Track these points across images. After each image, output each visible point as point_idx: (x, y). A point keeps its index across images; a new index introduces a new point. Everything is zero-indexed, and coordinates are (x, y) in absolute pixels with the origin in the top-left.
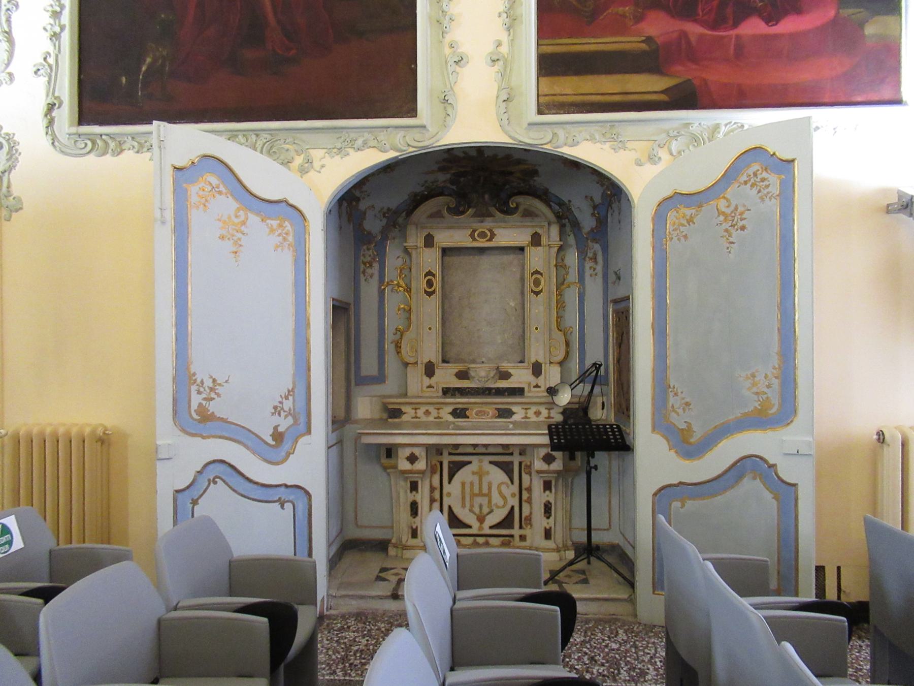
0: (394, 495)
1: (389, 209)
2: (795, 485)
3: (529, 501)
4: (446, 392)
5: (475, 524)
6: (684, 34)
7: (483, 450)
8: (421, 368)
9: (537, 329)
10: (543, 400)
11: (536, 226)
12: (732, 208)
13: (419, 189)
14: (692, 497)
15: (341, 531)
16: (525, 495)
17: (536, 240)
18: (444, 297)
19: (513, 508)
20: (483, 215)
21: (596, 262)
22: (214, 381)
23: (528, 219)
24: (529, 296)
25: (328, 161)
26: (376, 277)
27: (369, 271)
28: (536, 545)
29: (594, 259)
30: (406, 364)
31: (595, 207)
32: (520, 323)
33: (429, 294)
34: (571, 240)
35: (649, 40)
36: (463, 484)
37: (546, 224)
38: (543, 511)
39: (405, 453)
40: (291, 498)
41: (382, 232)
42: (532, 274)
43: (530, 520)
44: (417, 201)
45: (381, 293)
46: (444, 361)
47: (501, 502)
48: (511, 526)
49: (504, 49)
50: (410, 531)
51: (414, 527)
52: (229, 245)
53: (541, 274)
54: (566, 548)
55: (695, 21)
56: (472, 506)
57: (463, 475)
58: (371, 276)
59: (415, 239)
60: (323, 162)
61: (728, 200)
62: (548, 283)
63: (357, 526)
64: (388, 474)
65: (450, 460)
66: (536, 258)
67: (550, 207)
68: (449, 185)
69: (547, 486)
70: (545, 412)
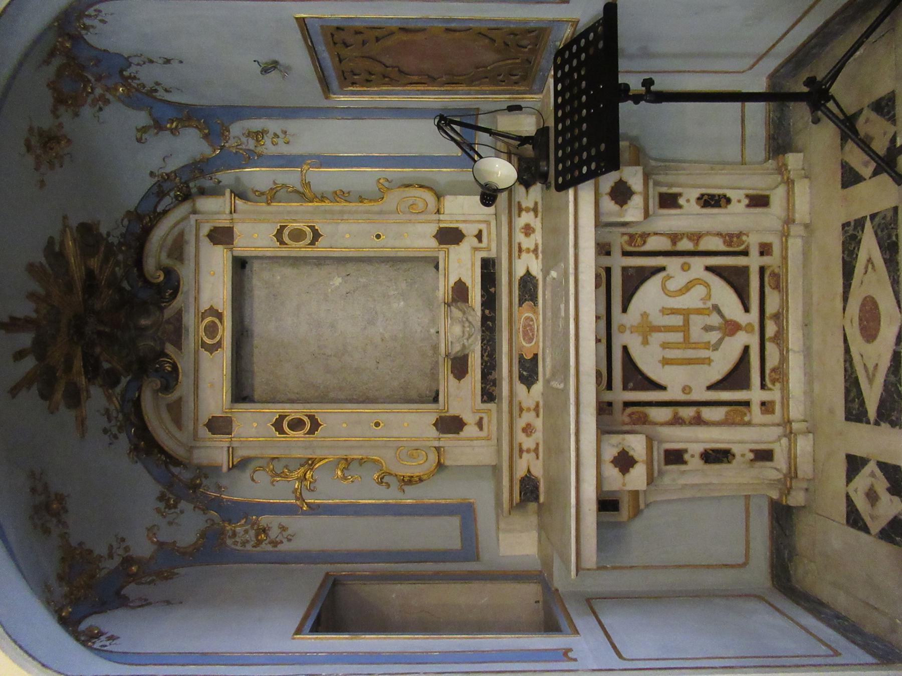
0: (688, 494)
1: (162, 498)
3: (696, 237)
4: (489, 394)
5: (741, 339)
8: (448, 441)
9: (378, 236)
10: (504, 219)
11: (198, 230)
13: (124, 442)
15: (760, 598)
16: (685, 245)
17: (222, 236)
18: (324, 399)
19: (708, 269)
20: (177, 333)
21: (263, 132)
24: (321, 249)
26: (284, 520)
27: (274, 533)
28: (778, 225)
29: (258, 135)
30: (440, 466)
31: (158, 126)
32: (369, 268)
34: (226, 177)
36: (666, 362)
37: (193, 218)
38: (715, 211)
39: (614, 478)
41: (205, 510)
42: (282, 243)
43: (731, 236)
44: (146, 445)
45: (315, 510)
46: (436, 400)
47: (700, 290)
48: (744, 271)
51: (751, 456)
53: (283, 228)
54: (782, 169)
56: (707, 346)
57: (648, 362)
58: (283, 528)
59: (215, 451)
62: (299, 214)
63: (744, 565)
64: (647, 506)
65: (626, 388)
67: (165, 212)
68: (119, 389)
69: (669, 201)
70: (527, 218)
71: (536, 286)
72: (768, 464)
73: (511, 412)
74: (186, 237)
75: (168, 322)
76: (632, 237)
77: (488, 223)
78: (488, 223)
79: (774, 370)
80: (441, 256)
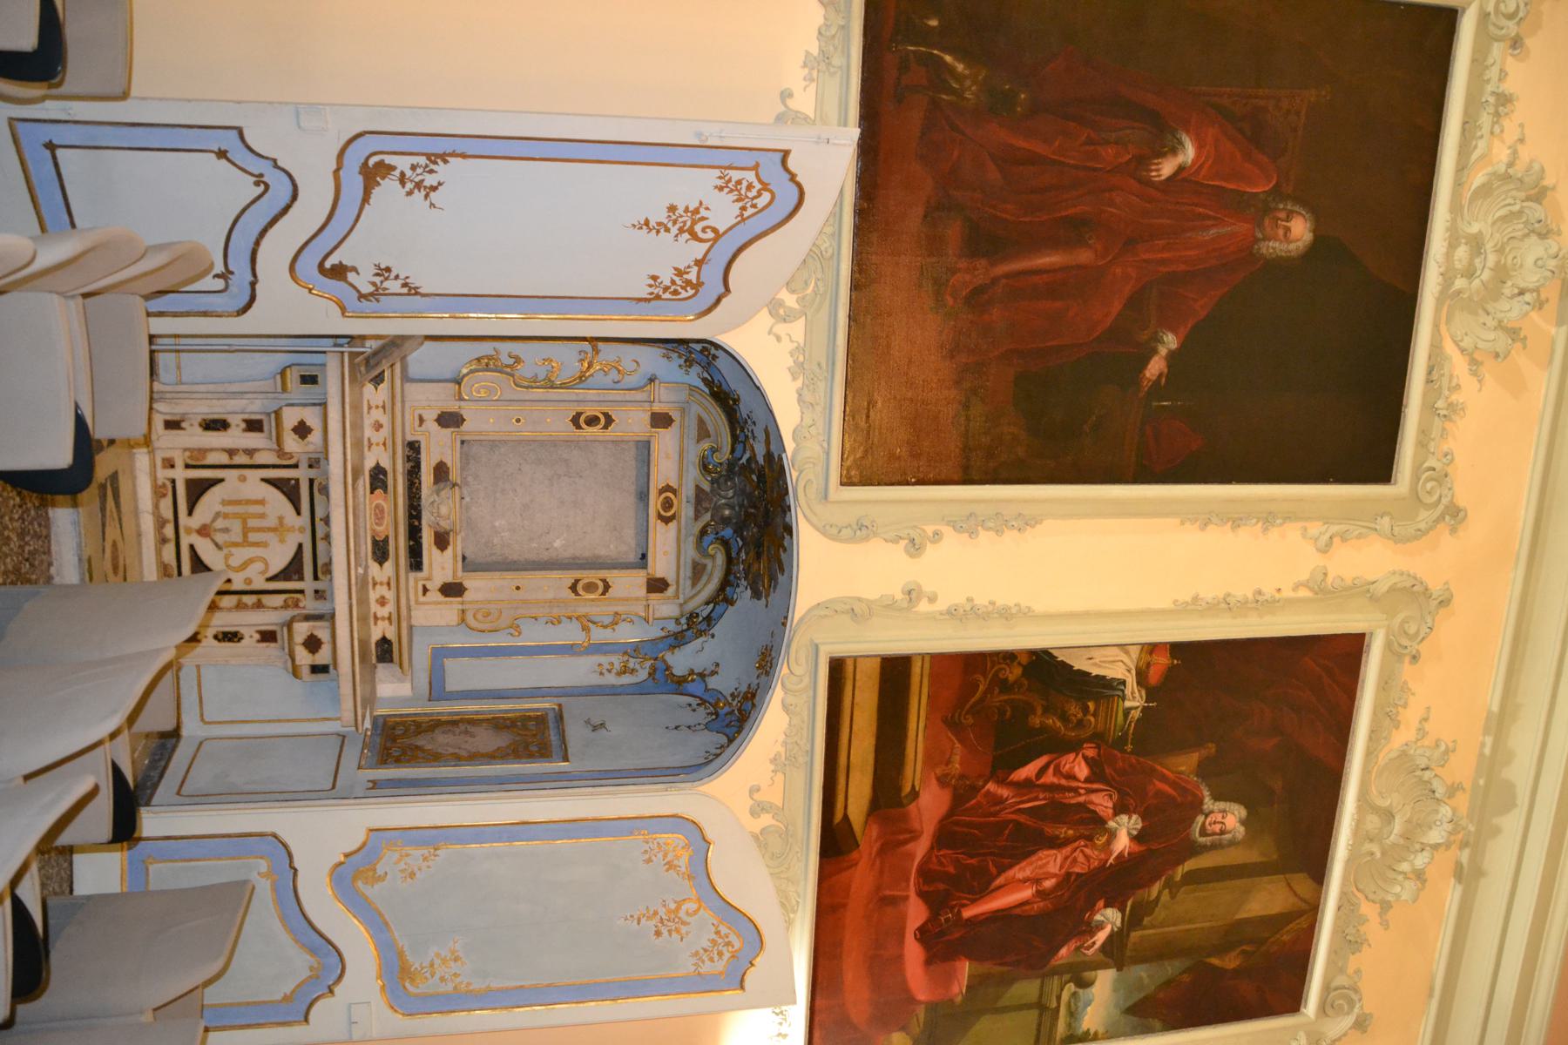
2: (306, 1020)
4: (414, 448)
6: (915, 836)
7: (320, 534)
8: (452, 406)
12: (687, 919)
14: (275, 889)
16: (249, 600)
17: (657, 586)
18: (568, 442)
21: (619, 674)
22: (434, 189)
23: (689, 573)
24: (568, 577)
25: (787, 346)
29: (625, 671)
31: (702, 675)
33: (575, 421)
34: (655, 632)
35: (915, 794)
36: (262, 502)
40: (233, 289)
49: (923, 606)
50: (177, 418)
51: (183, 425)
52: (662, 216)
53: (604, 593)
55: (932, 848)
56: (226, 516)
60: (785, 339)
61: (696, 912)
66: (629, 584)
67: (707, 603)
70: (383, 612)
71: (374, 553)
72: (168, 418)
73: (394, 443)
74: (689, 583)
75: (707, 510)
76: (297, 606)
77: (417, 602)
78: (417, 602)
79: (164, 495)
80: (460, 573)
